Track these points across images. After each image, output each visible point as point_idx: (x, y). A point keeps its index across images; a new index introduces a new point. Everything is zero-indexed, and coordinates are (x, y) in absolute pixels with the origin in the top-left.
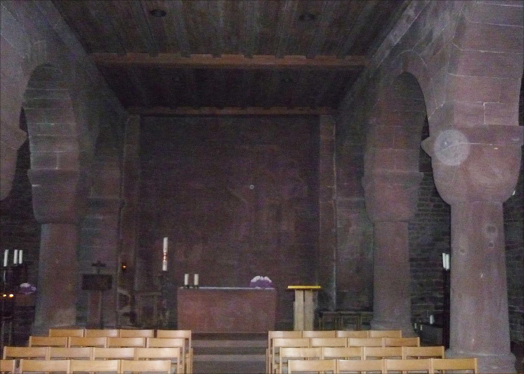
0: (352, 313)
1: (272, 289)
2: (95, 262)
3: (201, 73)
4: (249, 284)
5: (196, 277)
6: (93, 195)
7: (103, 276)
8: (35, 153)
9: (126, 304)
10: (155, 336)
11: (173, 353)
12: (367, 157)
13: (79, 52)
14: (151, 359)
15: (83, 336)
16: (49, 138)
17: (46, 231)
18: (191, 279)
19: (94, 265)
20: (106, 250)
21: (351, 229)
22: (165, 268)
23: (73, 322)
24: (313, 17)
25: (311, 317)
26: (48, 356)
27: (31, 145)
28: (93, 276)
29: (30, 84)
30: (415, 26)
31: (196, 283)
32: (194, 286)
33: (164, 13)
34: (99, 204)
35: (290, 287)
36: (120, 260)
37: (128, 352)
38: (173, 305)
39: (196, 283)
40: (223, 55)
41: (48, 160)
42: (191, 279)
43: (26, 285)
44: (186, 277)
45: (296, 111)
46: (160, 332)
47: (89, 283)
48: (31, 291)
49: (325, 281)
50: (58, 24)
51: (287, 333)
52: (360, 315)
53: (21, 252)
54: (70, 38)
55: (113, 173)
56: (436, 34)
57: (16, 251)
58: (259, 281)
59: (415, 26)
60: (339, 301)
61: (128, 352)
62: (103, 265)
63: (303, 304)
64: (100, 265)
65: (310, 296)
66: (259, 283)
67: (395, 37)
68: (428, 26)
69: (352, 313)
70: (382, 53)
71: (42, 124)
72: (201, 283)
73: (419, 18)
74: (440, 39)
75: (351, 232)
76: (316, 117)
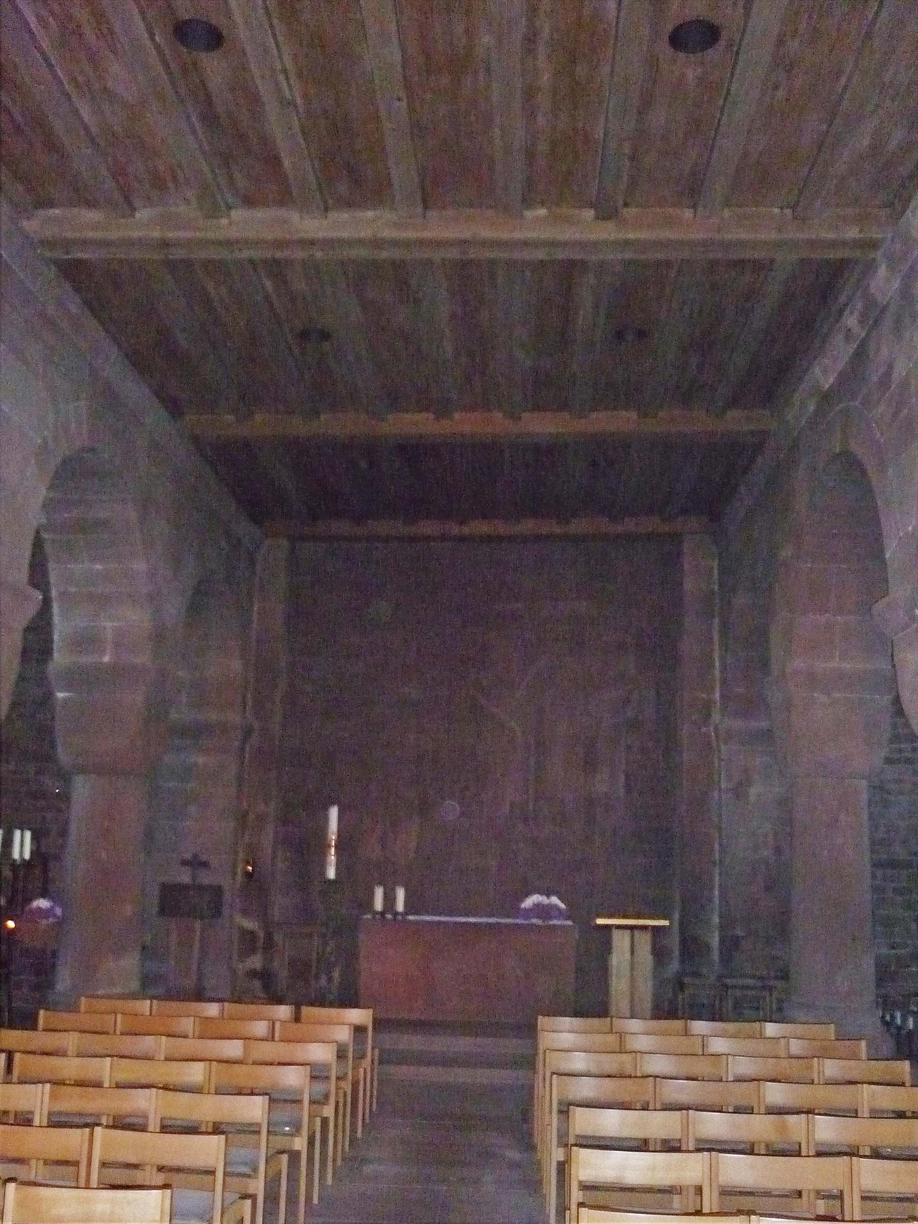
0: (750, 982)
1: (569, 923)
2: (188, 856)
3: (412, 451)
4: (516, 911)
5: (401, 894)
6: (181, 714)
7: (201, 888)
8: (61, 628)
9: (253, 951)
10: (297, 1019)
11: (321, 1053)
12: (775, 635)
13: (155, 417)
14: (280, 1064)
15: (148, 1013)
16: (91, 597)
17: (82, 789)
18: (389, 899)
19: (184, 863)
20: (210, 829)
21: (753, 791)
22: (331, 874)
23: (135, 985)
24: (641, 334)
25: (646, 989)
26: (71, 1050)
27: (55, 609)
28: (186, 887)
29: (51, 487)
30: (861, 354)
31: (400, 906)
32: (396, 914)
33: (325, 336)
34: (196, 733)
35: (600, 921)
36: (241, 855)
37: (233, 1049)
38: (351, 956)
39: (400, 906)
40: (457, 416)
41: (85, 641)
42: (389, 899)
43: (42, 903)
44: (379, 893)
45: (629, 525)
46: (306, 1010)
47: (173, 902)
48: (55, 916)
49: (693, 908)
50: (114, 367)
51: (595, 1022)
52: (771, 989)
53: (28, 835)
54: (135, 391)
55: (228, 665)
56: (900, 370)
57: (17, 834)
58: (537, 906)
59: (861, 354)
60: (727, 957)
61: (233, 1049)
62: (205, 865)
63: (629, 960)
64: (197, 863)
65: (644, 942)
66: (542, 911)
67: (824, 373)
68: (885, 351)
69: (750, 982)
70: (801, 407)
71: (79, 568)
72: (411, 907)
73: (868, 335)
74: (905, 384)
75: (752, 799)
76: (676, 538)
